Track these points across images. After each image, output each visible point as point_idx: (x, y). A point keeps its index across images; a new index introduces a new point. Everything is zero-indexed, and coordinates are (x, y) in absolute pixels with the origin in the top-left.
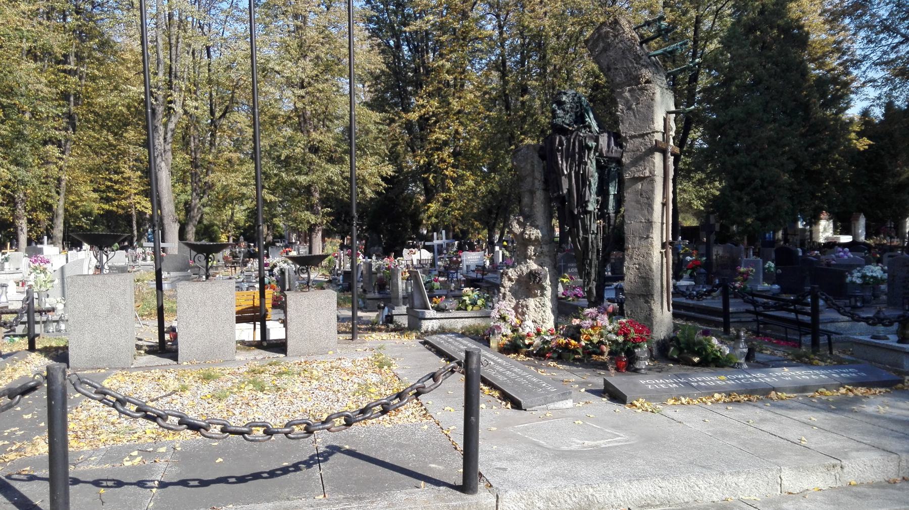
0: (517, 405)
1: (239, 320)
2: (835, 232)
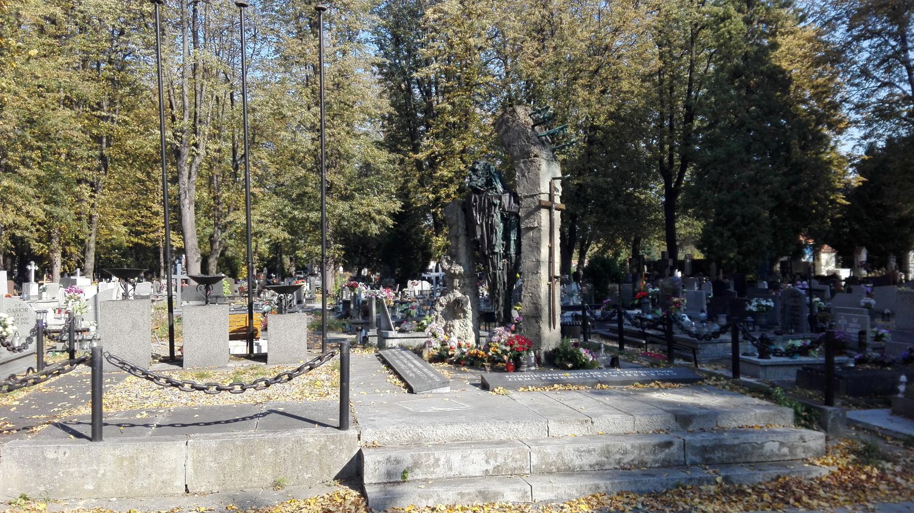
0: (411, 391)
1: (232, 338)
2: (837, 266)
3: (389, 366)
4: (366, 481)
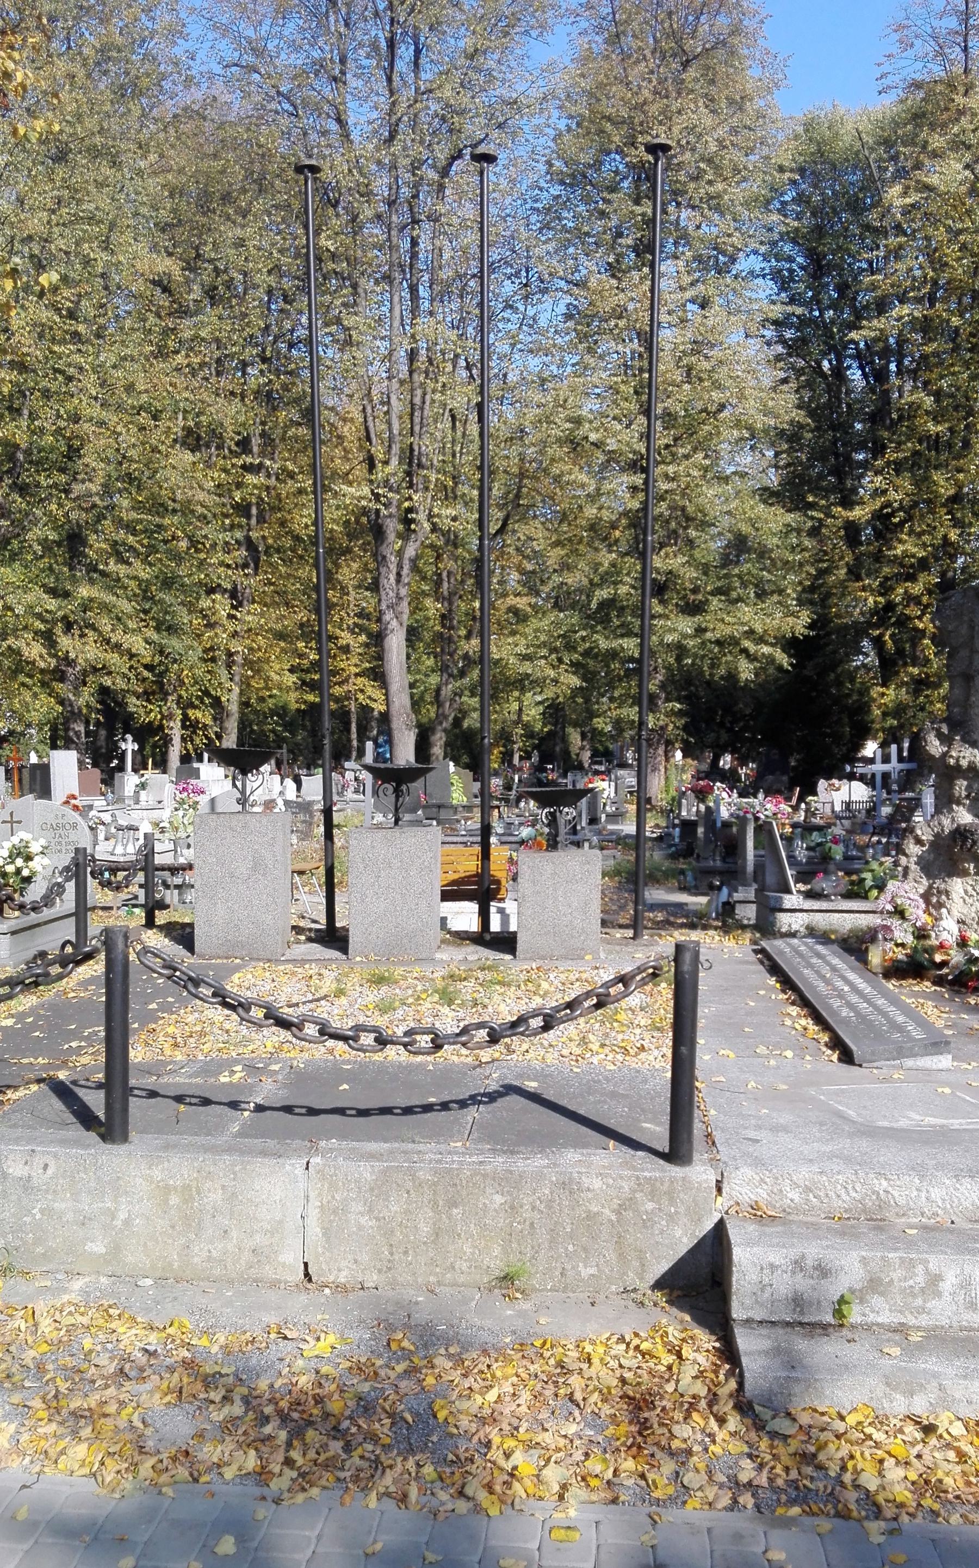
0: (847, 1057)
1: (447, 896)
3: (787, 983)
4: (738, 1312)
